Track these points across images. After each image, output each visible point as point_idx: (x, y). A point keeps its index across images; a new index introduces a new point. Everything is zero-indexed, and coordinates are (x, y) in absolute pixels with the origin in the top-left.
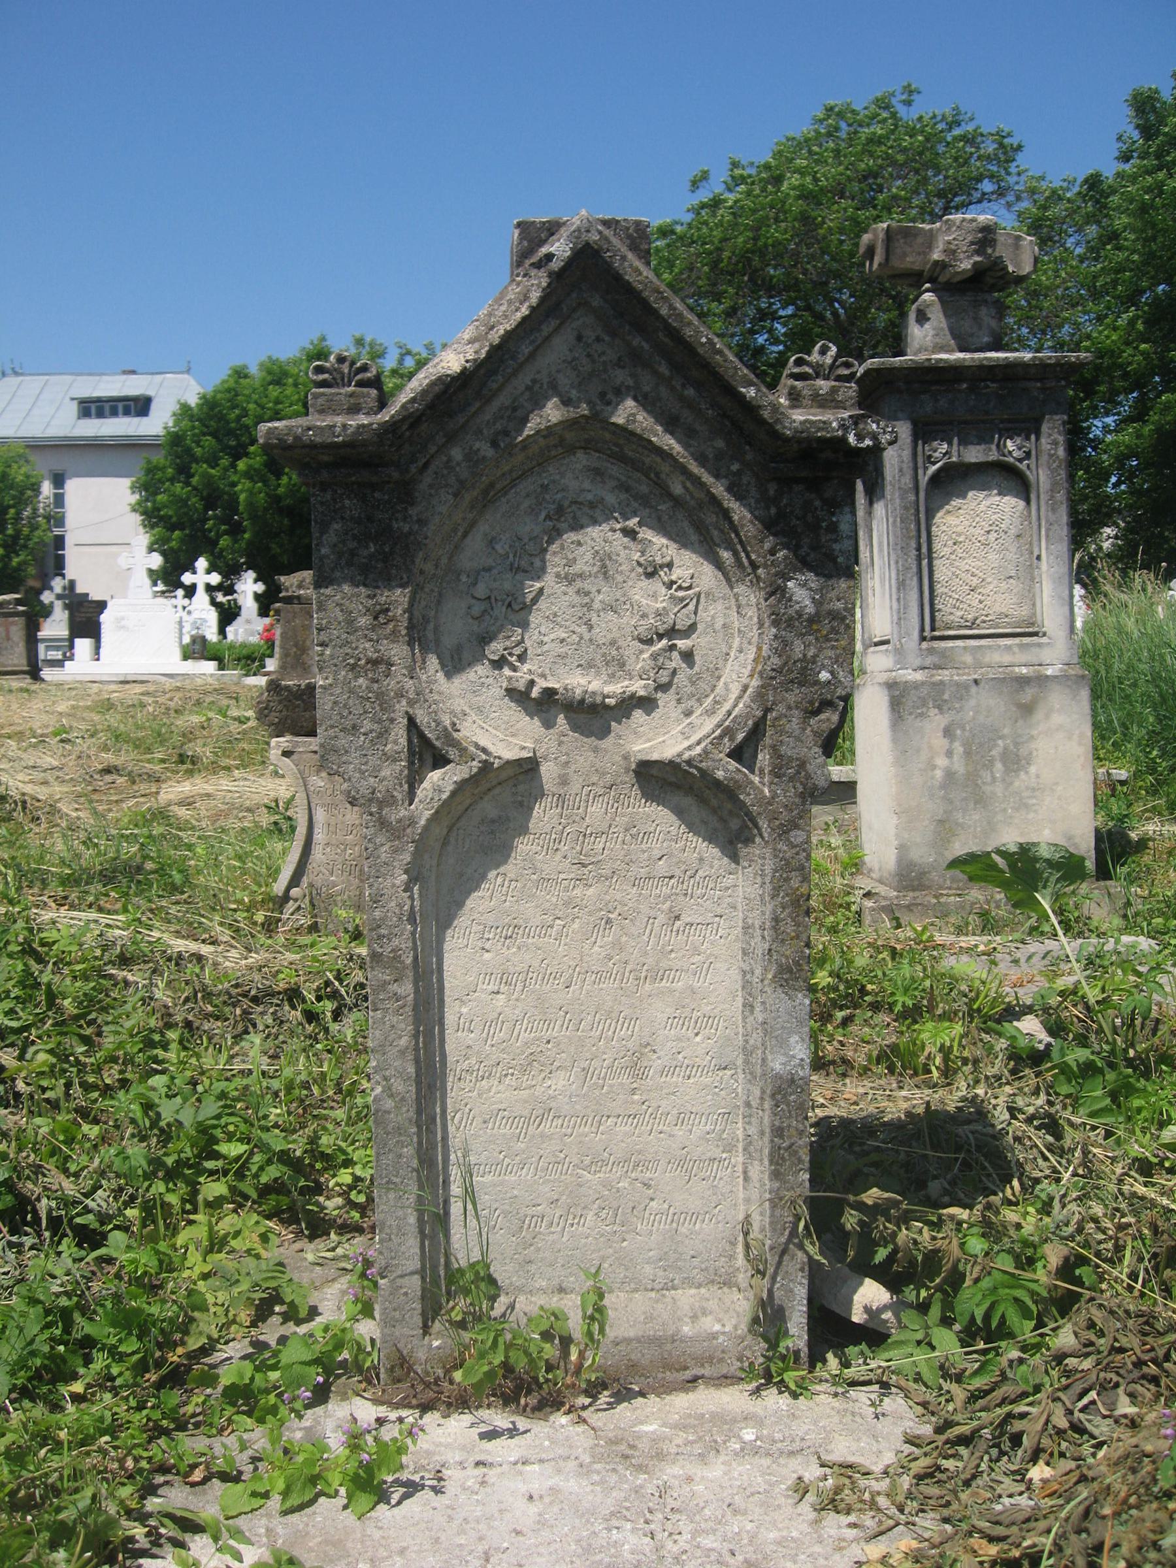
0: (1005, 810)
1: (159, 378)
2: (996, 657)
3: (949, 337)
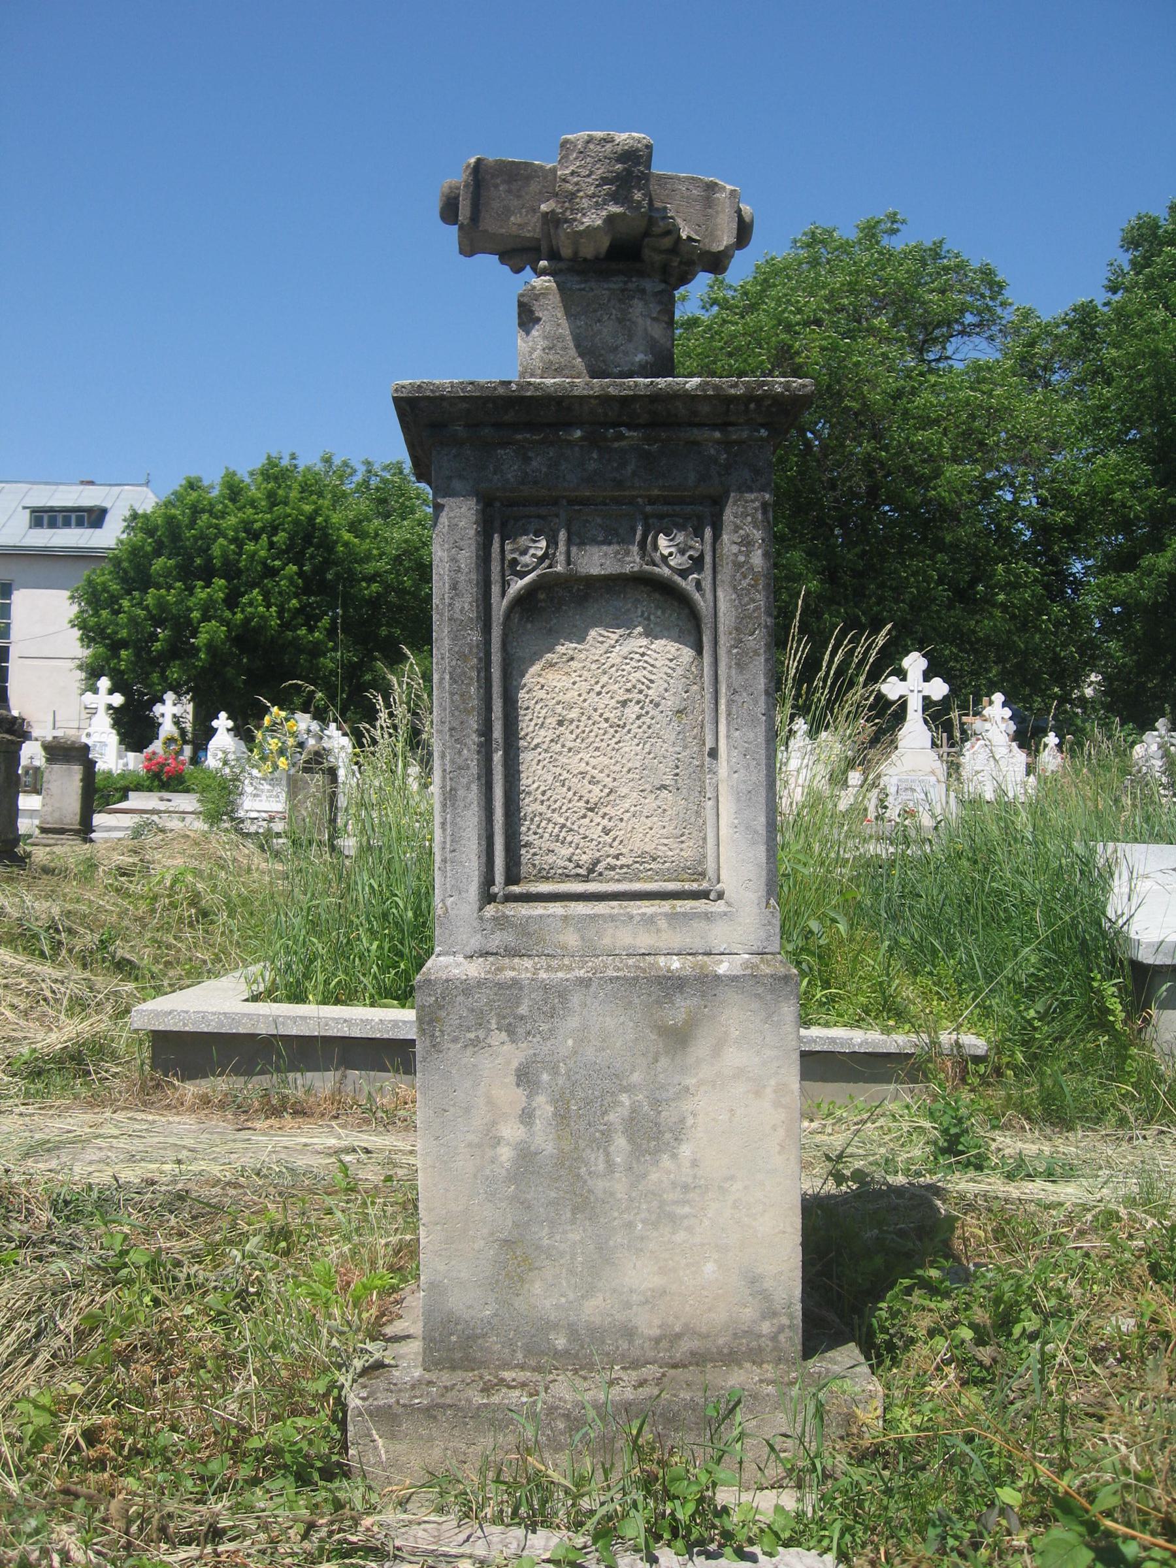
0: (630, 1225)
1: (117, 489)
2: (625, 937)
3: (573, 352)
